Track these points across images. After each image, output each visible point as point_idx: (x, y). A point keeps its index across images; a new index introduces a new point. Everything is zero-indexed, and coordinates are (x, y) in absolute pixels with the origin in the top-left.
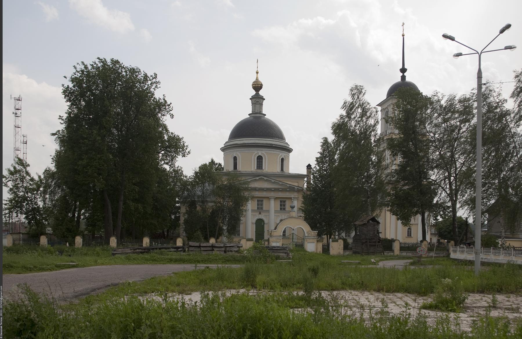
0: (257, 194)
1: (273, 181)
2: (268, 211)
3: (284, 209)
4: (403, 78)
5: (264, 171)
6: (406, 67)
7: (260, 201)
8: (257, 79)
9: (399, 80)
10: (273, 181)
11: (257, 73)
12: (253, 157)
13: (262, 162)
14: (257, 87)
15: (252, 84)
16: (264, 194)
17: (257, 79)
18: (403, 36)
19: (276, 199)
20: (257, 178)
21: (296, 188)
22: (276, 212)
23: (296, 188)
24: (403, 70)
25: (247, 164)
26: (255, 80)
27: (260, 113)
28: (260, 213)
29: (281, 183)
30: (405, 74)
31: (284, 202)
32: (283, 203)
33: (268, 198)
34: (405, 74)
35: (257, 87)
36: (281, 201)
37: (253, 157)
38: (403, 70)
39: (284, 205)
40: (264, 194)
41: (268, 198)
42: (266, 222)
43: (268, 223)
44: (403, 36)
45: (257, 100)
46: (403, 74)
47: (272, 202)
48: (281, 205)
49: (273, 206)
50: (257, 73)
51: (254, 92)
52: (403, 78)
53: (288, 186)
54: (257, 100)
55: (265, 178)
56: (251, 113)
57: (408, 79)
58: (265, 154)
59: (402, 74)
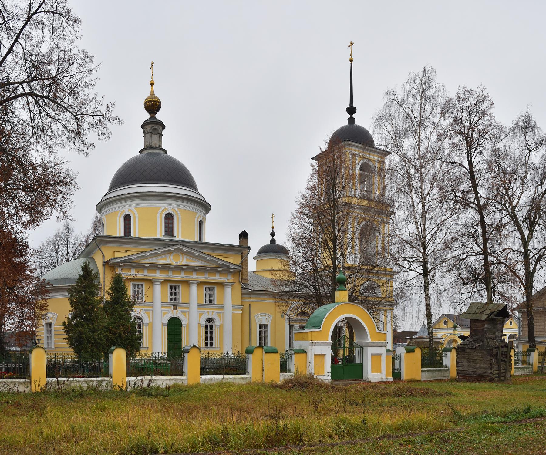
0: (170, 275)
1: (197, 254)
2: (187, 305)
3: (211, 301)
4: (351, 120)
5: (177, 239)
6: (354, 105)
7: (174, 288)
8: (152, 93)
9: (346, 123)
10: (197, 254)
11: (152, 84)
12: (158, 215)
13: (172, 224)
14: (153, 106)
15: (144, 102)
16: (182, 276)
17: (152, 93)
18: (351, 61)
19: (164, 282)
20: (172, 249)
21: (232, 267)
22: (200, 306)
23: (232, 267)
24: (351, 110)
25: (148, 223)
26: (148, 94)
27: (160, 148)
28: (175, 308)
29: (209, 258)
30: (354, 116)
31: (177, 288)
32: (174, 291)
33: (187, 283)
34: (354, 116)
35: (153, 106)
36: (171, 287)
37: (158, 215)
38: (351, 110)
39: (176, 294)
40: (182, 276)
41: (187, 283)
42: (184, 322)
43: (188, 325)
44: (351, 61)
45: (153, 128)
46: (351, 116)
47: (194, 289)
48: (171, 294)
49: (195, 295)
50: (152, 84)
51: (147, 116)
52: (351, 120)
53: (220, 262)
54: (153, 128)
55: (185, 249)
56: (143, 147)
57: (357, 123)
58: (177, 210)
59: (349, 116)
